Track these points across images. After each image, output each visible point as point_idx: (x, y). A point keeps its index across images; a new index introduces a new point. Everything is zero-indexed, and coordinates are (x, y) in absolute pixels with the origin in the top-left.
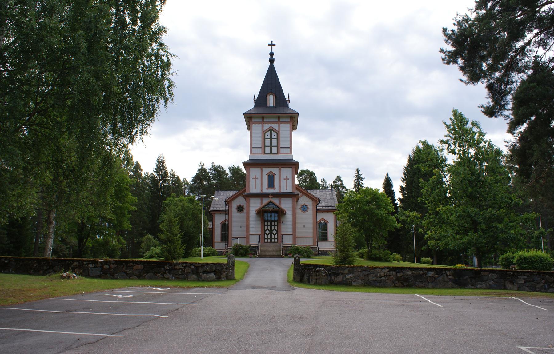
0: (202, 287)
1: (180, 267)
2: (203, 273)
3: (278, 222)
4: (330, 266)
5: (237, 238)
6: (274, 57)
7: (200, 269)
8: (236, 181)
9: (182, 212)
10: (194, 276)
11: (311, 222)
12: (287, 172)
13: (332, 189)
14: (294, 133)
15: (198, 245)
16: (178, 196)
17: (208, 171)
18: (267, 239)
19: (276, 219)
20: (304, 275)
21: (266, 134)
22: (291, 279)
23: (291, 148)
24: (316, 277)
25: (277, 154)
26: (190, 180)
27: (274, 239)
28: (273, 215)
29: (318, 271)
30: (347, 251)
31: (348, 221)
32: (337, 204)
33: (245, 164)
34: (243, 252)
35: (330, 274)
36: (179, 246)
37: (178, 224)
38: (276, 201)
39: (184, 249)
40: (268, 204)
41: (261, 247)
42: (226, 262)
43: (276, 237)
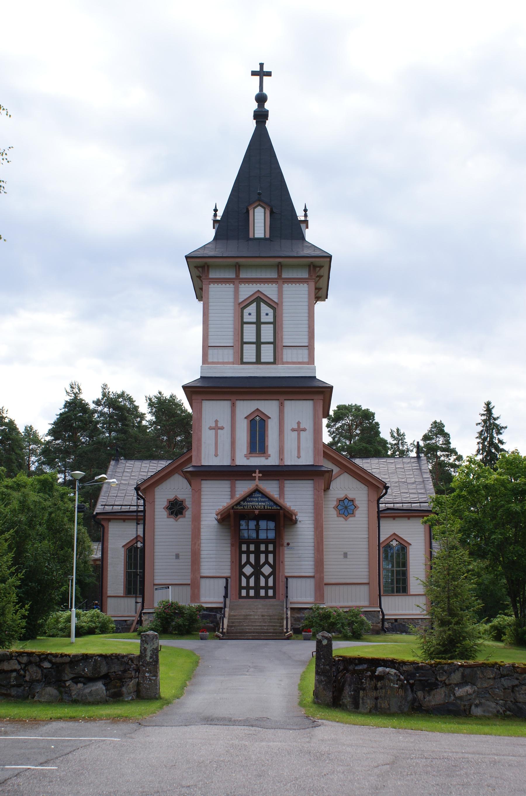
0: (73, 719)
1: (14, 665)
2: (76, 680)
3: (277, 544)
4: (413, 663)
5: (167, 586)
6: (267, 106)
7: (68, 670)
8: (168, 432)
9: (23, 518)
10: (51, 690)
11: (363, 545)
12: (299, 411)
13: (418, 457)
14: (319, 306)
15: (64, 603)
16: (11, 474)
17: (92, 406)
18: (248, 588)
19: (271, 535)
20: (345, 687)
21: (246, 311)
22: (310, 697)
23: (310, 347)
24: (374, 694)
25: (274, 363)
26: (43, 429)
27: (266, 588)
28: (263, 524)
29: (380, 678)
30: (457, 623)
31: (463, 542)
32: (434, 495)
33: (190, 390)
34: (180, 622)
35: (412, 686)
36: (11, 608)
37: (10, 547)
38: (271, 488)
39: (24, 617)
40: (250, 495)
41: (231, 609)
42: (137, 652)
43: (271, 583)
